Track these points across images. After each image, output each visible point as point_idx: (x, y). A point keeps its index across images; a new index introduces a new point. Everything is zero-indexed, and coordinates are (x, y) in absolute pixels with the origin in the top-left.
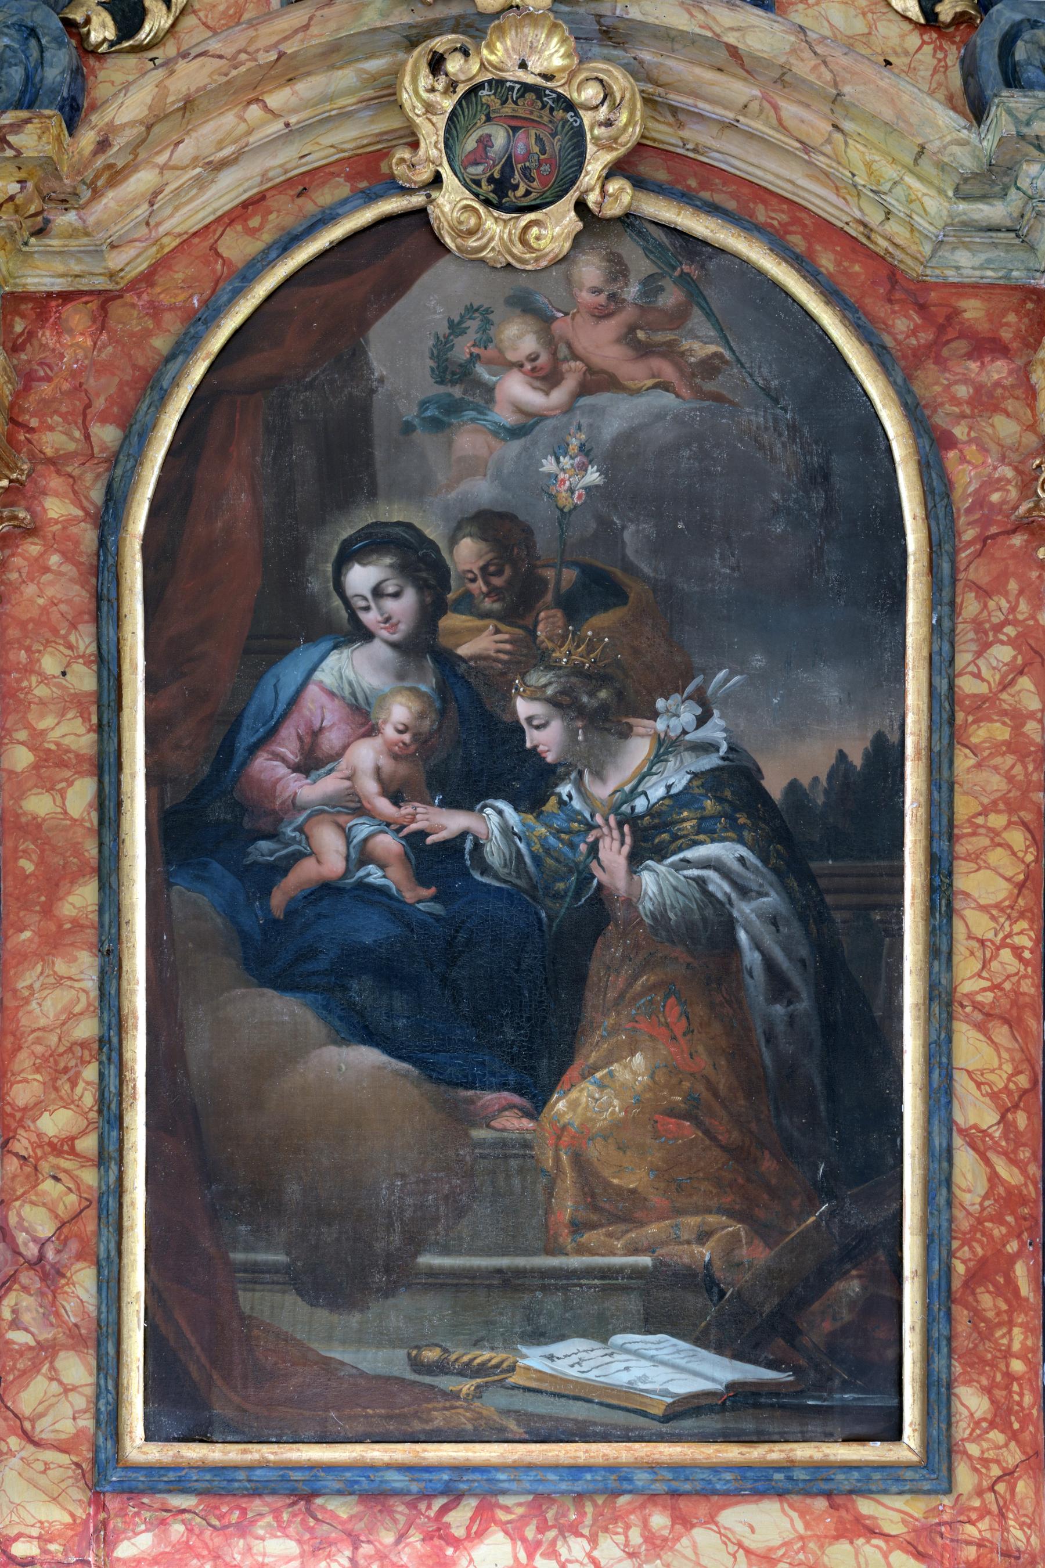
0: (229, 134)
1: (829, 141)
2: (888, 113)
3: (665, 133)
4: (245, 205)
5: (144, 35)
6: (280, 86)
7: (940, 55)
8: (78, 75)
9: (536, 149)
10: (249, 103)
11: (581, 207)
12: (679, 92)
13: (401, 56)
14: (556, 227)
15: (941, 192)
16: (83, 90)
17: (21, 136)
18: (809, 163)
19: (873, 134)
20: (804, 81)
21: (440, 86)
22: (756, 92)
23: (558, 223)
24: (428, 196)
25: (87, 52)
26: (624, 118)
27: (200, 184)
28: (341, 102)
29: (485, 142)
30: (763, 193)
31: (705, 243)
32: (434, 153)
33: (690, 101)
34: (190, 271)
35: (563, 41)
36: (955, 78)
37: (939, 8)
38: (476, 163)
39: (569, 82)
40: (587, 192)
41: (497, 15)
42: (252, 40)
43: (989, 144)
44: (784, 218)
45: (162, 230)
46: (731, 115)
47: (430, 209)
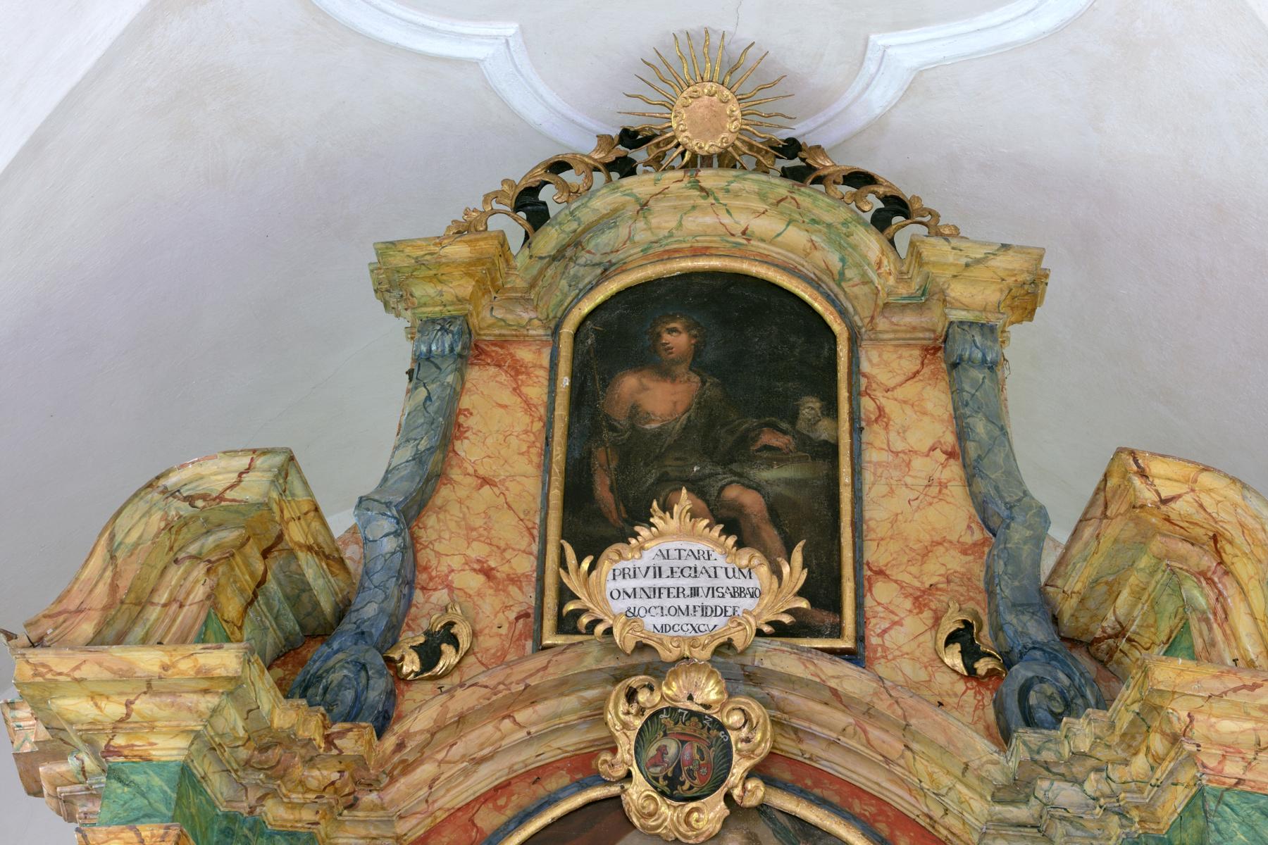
0: (488, 739)
1: (902, 756)
2: (941, 740)
3: (789, 746)
4: (496, 789)
5: (440, 668)
6: (526, 707)
7: (979, 698)
8: (391, 696)
9: (697, 757)
10: (504, 718)
11: (728, 798)
12: (799, 718)
13: (609, 688)
14: (711, 813)
15: (982, 796)
16: (394, 705)
17: (344, 740)
18: (889, 771)
19: (933, 753)
20: (883, 714)
21: (633, 711)
22: (851, 720)
23: (712, 809)
24: (622, 787)
25: (399, 679)
26: (758, 736)
27: (466, 773)
28: (567, 718)
29: (662, 751)
30: (858, 792)
31: (816, 827)
32: (627, 757)
33: (806, 724)
34: (453, 837)
35: (718, 683)
36: (990, 714)
37: (976, 665)
38: (656, 765)
39: (721, 710)
40: (733, 788)
41: (674, 663)
42: (508, 676)
43: (1013, 764)
44: (873, 810)
45: (436, 805)
46: (835, 735)
47: (623, 796)
